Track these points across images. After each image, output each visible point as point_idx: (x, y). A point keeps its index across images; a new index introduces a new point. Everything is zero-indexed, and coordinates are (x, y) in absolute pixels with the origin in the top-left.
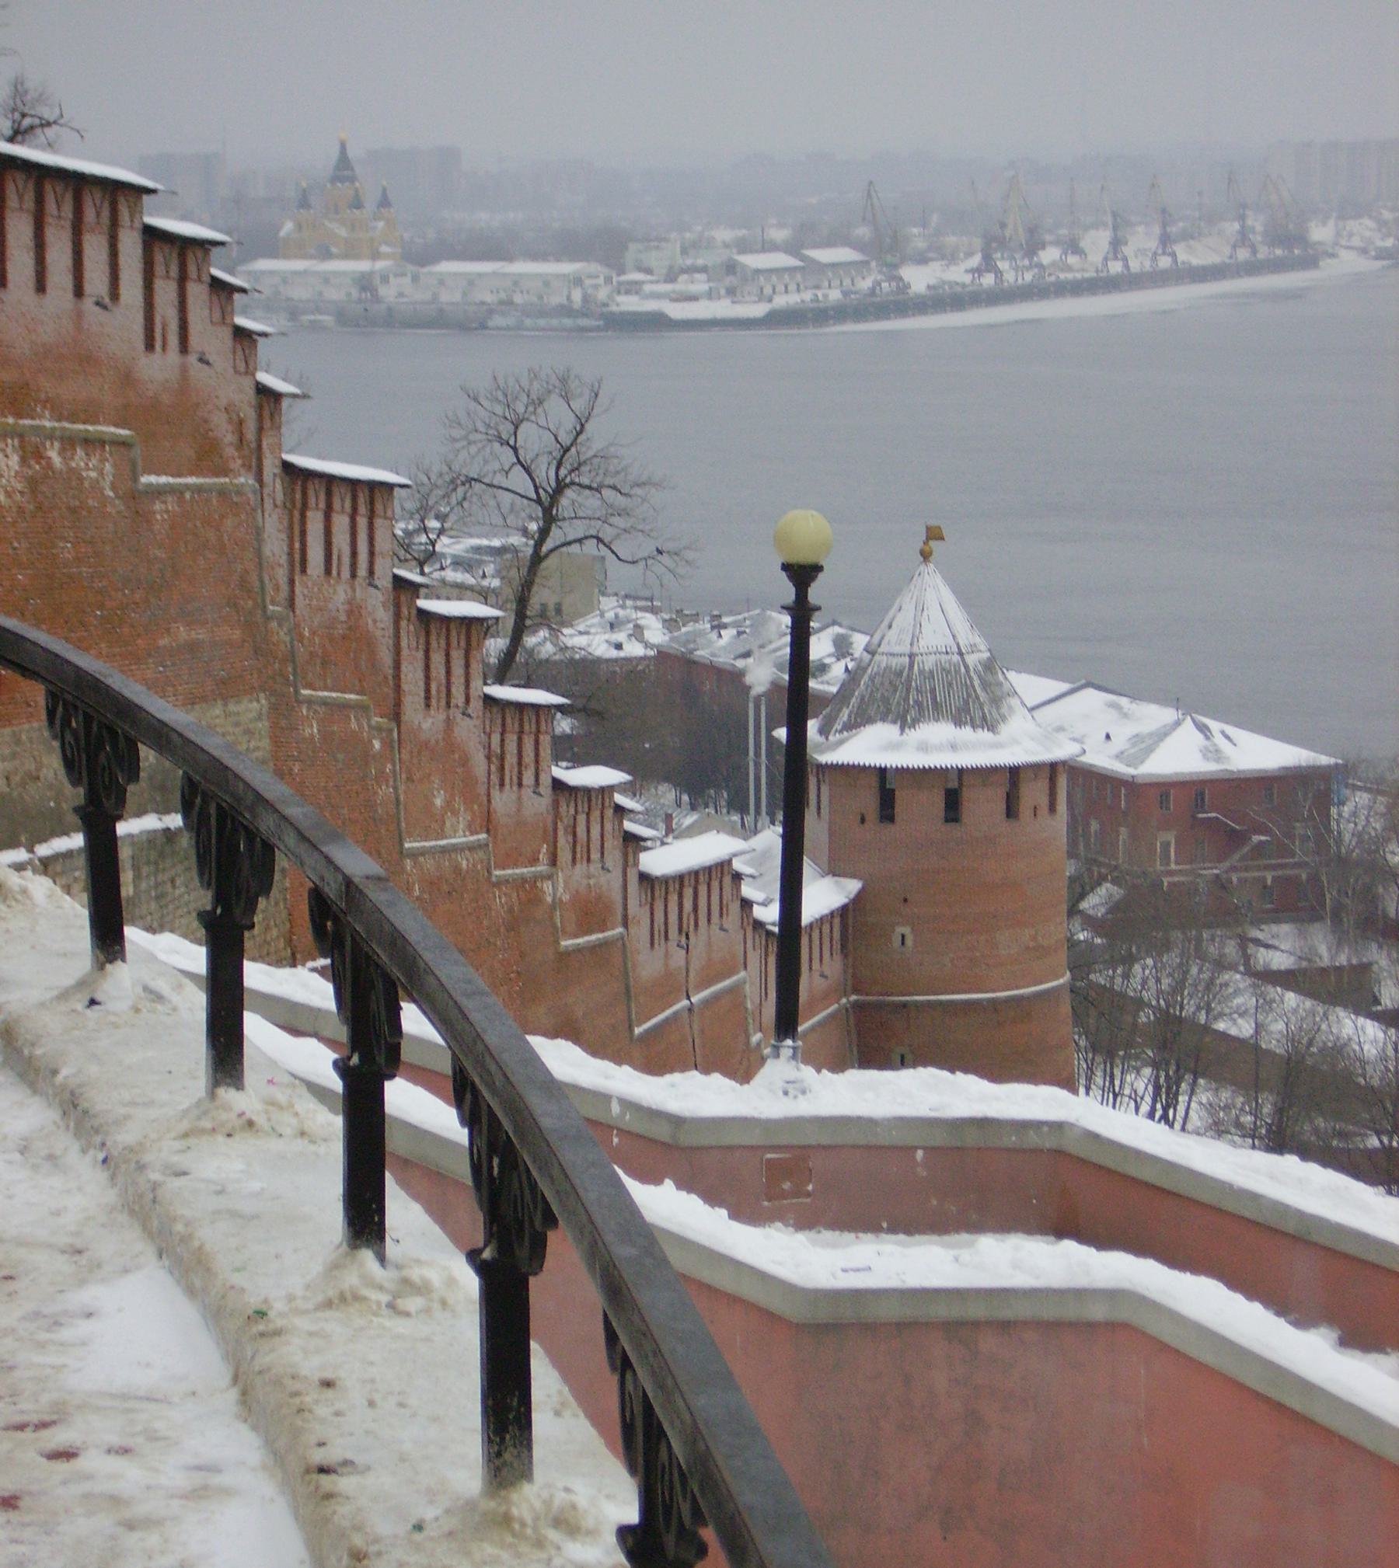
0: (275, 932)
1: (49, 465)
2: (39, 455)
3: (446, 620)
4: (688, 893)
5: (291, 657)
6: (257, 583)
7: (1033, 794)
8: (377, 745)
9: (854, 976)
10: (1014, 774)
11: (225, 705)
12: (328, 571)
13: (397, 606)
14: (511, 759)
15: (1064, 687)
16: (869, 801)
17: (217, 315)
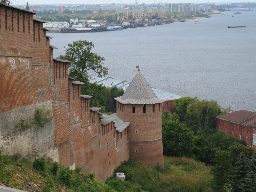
0: (53, 140)
1: (20, 62)
2: (18, 60)
3: (76, 85)
4: (107, 126)
5: (55, 93)
6: (50, 81)
7: (157, 108)
8: (66, 106)
9: (129, 137)
10: (154, 105)
11: (46, 102)
12: (60, 78)
13: (69, 82)
14: (84, 107)
15: (152, 89)
16: (131, 110)
17: (44, 36)
